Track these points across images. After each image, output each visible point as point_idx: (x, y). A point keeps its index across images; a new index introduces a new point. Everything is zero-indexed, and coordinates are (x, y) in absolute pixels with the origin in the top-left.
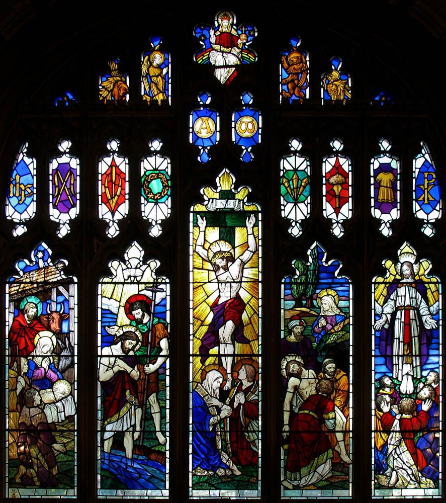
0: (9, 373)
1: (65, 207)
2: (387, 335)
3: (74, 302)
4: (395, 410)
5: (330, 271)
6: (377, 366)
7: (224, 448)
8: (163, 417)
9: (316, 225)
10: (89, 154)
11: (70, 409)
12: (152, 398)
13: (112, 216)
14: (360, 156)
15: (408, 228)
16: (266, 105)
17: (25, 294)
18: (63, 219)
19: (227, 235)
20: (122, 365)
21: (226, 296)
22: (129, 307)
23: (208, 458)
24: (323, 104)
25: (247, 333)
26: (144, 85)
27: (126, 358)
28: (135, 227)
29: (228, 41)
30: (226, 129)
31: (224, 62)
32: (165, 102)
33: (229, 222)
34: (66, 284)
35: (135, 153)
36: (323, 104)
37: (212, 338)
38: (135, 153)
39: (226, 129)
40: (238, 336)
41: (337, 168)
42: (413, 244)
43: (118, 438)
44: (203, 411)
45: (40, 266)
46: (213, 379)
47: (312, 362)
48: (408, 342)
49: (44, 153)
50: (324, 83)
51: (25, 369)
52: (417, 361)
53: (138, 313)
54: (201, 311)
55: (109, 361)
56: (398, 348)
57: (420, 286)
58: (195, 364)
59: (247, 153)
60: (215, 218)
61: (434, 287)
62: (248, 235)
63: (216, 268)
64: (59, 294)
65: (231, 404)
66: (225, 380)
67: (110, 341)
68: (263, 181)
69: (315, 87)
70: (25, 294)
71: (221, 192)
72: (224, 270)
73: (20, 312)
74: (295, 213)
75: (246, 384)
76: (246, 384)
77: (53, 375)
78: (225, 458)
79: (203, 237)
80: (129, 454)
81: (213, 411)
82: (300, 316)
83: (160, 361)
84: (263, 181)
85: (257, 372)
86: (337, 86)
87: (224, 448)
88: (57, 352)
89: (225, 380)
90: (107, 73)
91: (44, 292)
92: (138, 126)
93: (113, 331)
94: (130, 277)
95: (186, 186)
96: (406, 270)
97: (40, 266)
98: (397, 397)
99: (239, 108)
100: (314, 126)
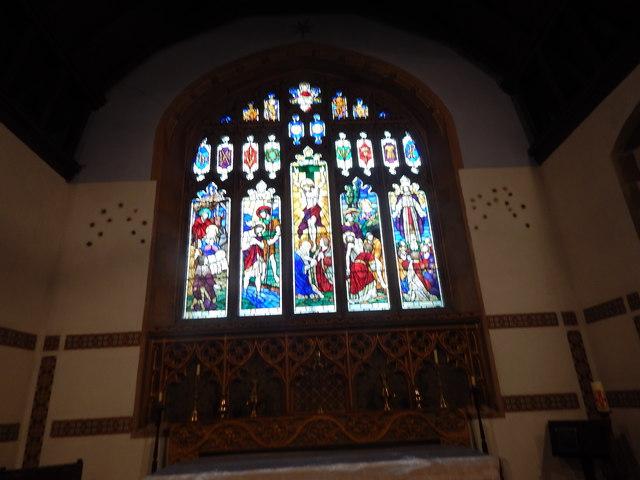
0: (191, 248)
1: (225, 165)
2: (400, 221)
3: (229, 211)
4: (409, 258)
5: (366, 191)
6: (396, 235)
7: (314, 283)
8: (278, 267)
9: (356, 171)
10: (238, 143)
11: (226, 266)
12: (272, 257)
13: (249, 170)
14: (376, 139)
15: (404, 170)
16: (327, 117)
17: (202, 207)
18: (367, 167)
19: (310, 175)
20: (255, 242)
21: (311, 205)
22: (259, 212)
23: (305, 288)
24: (198, 373)
25: (323, 222)
26: (266, 113)
27: (257, 238)
28: (262, 174)
29: (307, 94)
30: (307, 130)
31: (305, 103)
32: (276, 120)
33: (311, 170)
34: (224, 202)
35: (261, 140)
36: (198, 373)
37: (304, 225)
38: (261, 140)
39: (307, 130)
40: (318, 223)
41: (365, 145)
42: (408, 176)
43: (252, 283)
44: (300, 263)
45: (213, 194)
46: (306, 246)
47: (359, 234)
48: (411, 223)
49: (214, 142)
50: (354, 109)
51: (200, 245)
52: (418, 233)
53: (263, 214)
54: (297, 212)
55: (247, 241)
56: (406, 226)
57: (414, 196)
58: (295, 239)
59: (318, 140)
60: (304, 169)
61: (422, 195)
62: (322, 176)
63: (305, 192)
64: (220, 206)
65: (316, 258)
66: (312, 246)
67: (247, 229)
68: (327, 150)
69: (350, 110)
70: (202, 207)
71: (308, 156)
72: (310, 191)
73: (198, 216)
74: (345, 165)
75: (324, 248)
76: (324, 248)
77: (215, 248)
78: (314, 288)
79: (297, 178)
80: (259, 290)
81: (306, 263)
82: (351, 213)
83: (276, 238)
84: (327, 150)
85: (329, 241)
86: (361, 110)
87: (314, 283)
88: (218, 236)
89: (312, 246)
90: (247, 108)
91: (212, 206)
92: (261, 130)
93: (249, 224)
94: (260, 197)
95: (289, 152)
96: (406, 189)
97: (213, 194)
98: (409, 252)
99: (313, 120)
100: (352, 127)
